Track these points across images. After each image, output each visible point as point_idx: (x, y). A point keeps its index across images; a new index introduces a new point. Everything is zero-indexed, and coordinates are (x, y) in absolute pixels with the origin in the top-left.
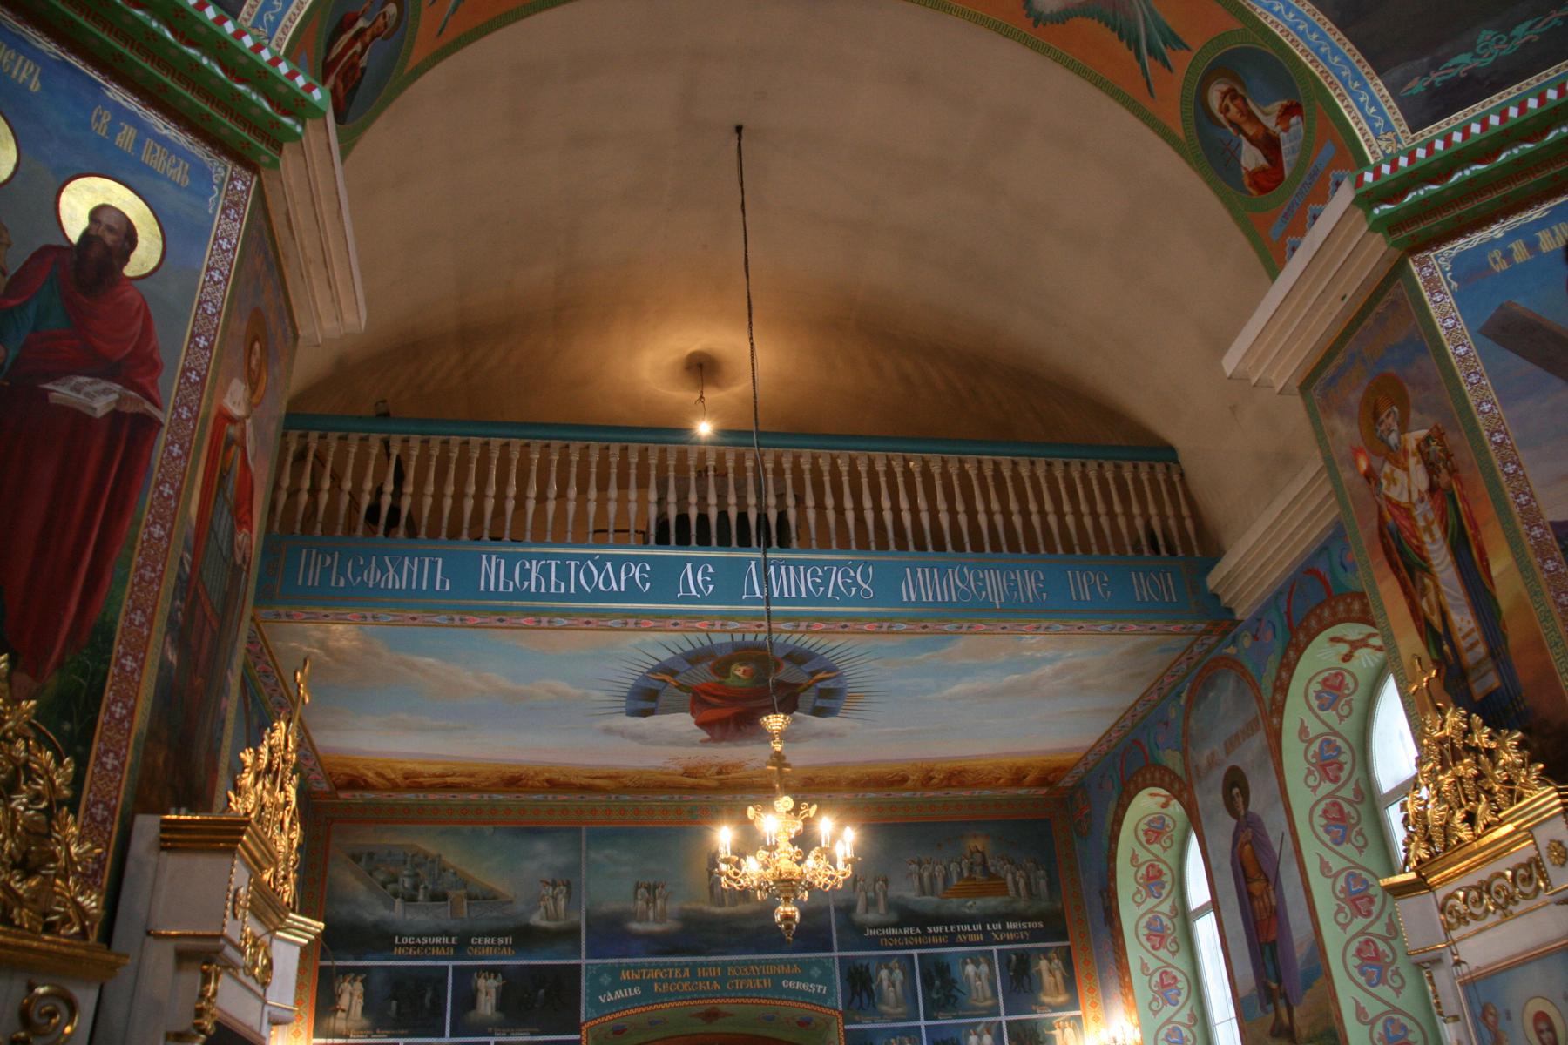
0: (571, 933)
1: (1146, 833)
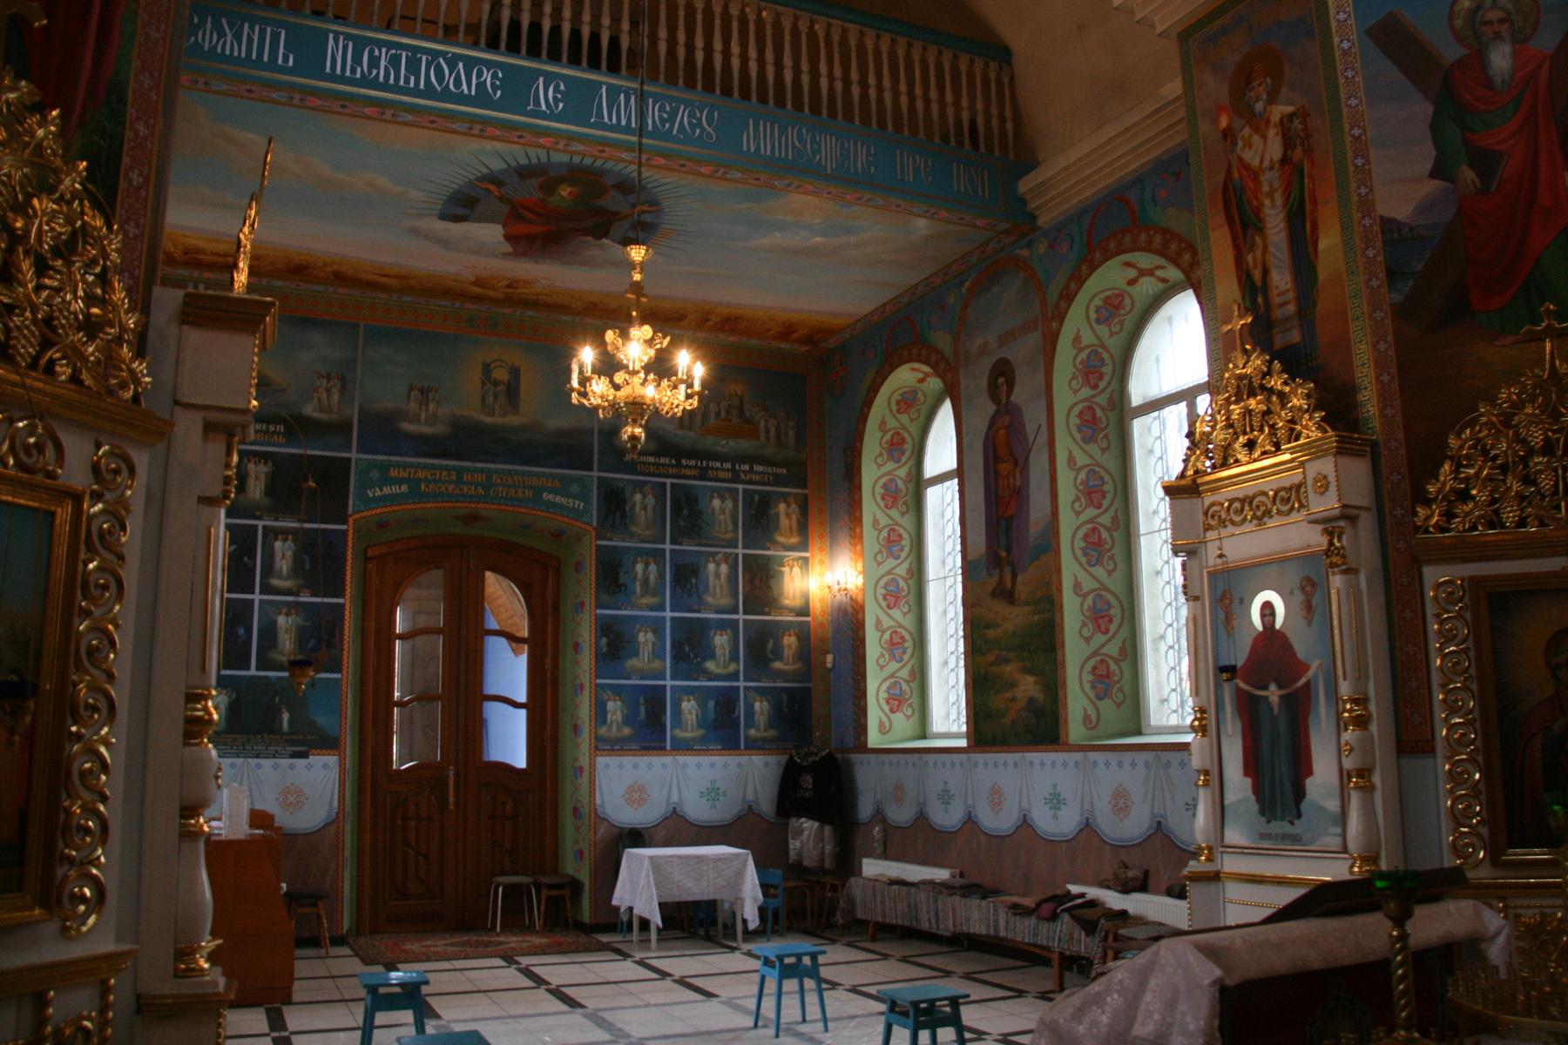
0: (343, 428)
1: (898, 403)
